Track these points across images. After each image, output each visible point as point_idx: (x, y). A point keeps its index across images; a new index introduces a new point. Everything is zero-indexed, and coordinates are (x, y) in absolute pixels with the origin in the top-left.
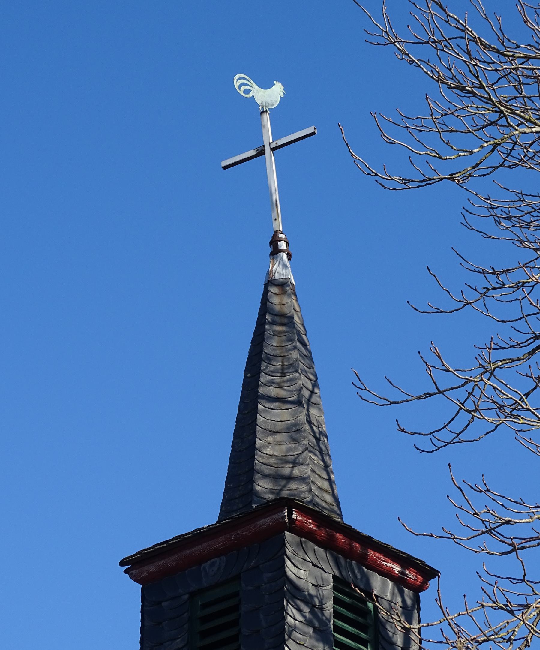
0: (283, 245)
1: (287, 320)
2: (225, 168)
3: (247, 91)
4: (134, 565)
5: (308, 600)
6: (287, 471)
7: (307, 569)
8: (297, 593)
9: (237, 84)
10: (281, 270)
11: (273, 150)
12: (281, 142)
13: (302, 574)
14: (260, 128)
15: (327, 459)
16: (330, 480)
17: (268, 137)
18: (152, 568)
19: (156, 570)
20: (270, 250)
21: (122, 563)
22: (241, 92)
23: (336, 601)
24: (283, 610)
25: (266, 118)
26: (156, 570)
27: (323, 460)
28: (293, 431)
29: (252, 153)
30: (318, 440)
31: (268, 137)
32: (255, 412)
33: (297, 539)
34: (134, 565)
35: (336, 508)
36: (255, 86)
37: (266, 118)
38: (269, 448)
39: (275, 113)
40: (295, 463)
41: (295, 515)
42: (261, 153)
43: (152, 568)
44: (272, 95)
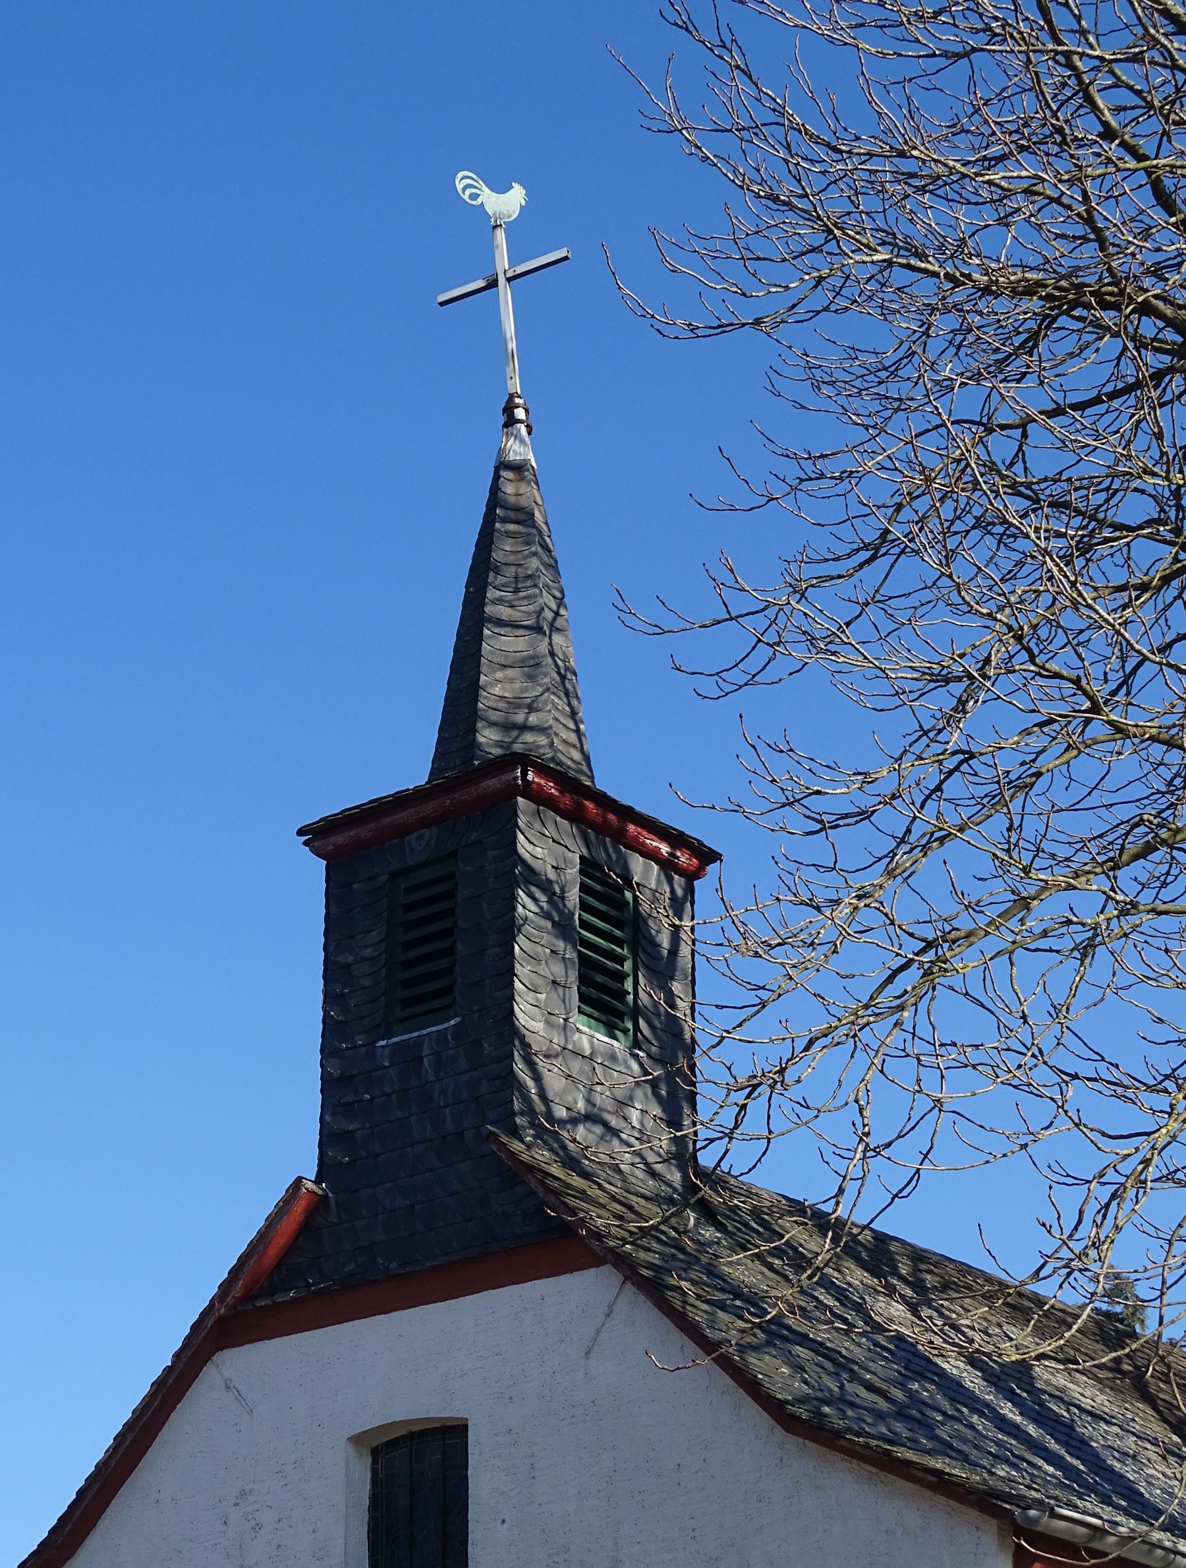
0: (520, 414)
1: (525, 516)
2: (442, 304)
3: (474, 197)
4: (317, 835)
5: (546, 886)
6: (520, 718)
7: (546, 846)
8: (531, 877)
9: (459, 186)
10: (518, 449)
11: (509, 280)
12: (520, 269)
13: (538, 852)
14: (491, 248)
15: (575, 703)
16: (578, 731)
17: (503, 262)
18: (340, 839)
19: (350, 844)
20: (502, 419)
21: (300, 832)
22: (466, 198)
23: (584, 888)
24: (514, 898)
25: (501, 236)
26: (350, 844)
27: (569, 705)
28: (531, 666)
29: (481, 283)
30: (563, 677)
31: (503, 262)
32: (480, 638)
33: (533, 806)
34: (317, 835)
35: (585, 768)
36: (485, 189)
37: (501, 236)
38: (497, 687)
39: (512, 228)
40: (531, 708)
41: (530, 776)
42: (493, 284)
43: (340, 839)
44: (510, 202)
